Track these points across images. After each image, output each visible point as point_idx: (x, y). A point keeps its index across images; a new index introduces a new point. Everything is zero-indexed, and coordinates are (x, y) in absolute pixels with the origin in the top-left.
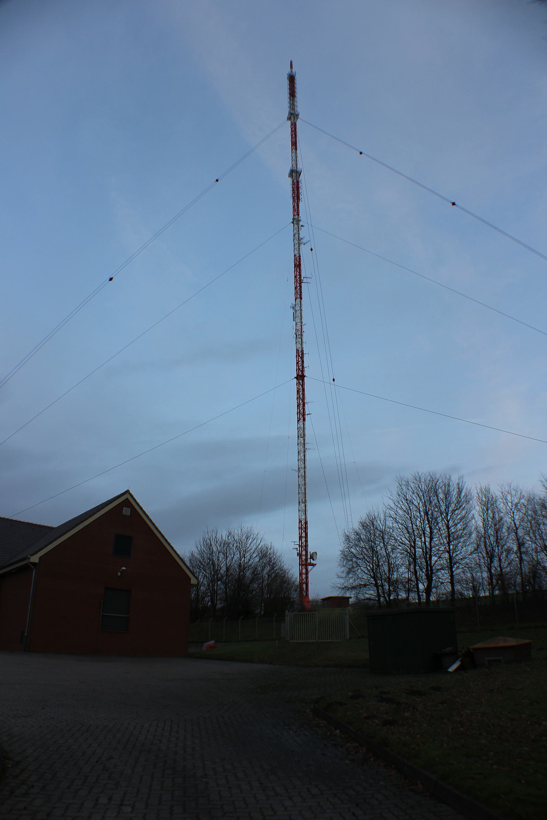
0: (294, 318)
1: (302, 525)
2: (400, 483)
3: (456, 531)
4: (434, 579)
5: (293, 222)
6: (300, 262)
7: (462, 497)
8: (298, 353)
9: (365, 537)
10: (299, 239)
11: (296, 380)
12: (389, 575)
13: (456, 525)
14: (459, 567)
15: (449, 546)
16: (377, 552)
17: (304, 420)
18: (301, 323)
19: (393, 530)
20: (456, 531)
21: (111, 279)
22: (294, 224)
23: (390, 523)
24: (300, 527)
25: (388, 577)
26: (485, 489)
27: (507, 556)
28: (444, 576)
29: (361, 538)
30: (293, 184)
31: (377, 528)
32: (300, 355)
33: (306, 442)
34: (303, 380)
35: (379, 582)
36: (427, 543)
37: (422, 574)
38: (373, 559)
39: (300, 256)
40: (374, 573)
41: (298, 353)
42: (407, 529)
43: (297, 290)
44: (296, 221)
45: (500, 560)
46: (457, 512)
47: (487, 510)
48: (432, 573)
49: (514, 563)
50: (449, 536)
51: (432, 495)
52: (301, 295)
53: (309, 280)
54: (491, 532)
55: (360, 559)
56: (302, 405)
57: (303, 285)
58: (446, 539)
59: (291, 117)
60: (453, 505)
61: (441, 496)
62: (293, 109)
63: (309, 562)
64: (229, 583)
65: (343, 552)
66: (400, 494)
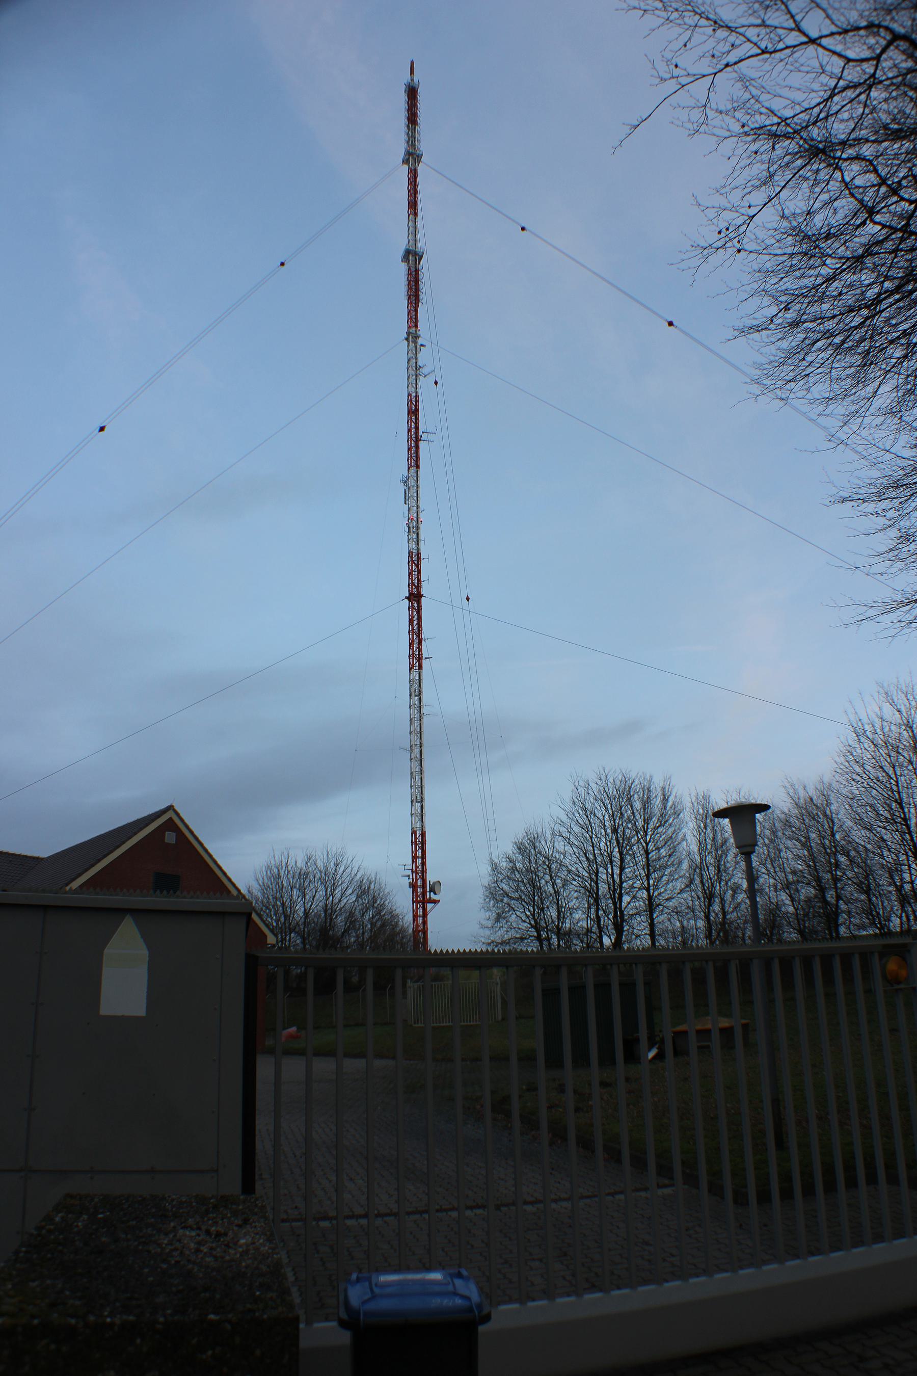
0: (405, 498)
1: (416, 838)
2: (576, 784)
3: (659, 859)
4: (625, 929)
5: (407, 339)
6: (417, 405)
7: (668, 808)
9: (521, 866)
10: (417, 368)
11: (407, 601)
12: (559, 923)
13: (658, 849)
14: (662, 911)
15: (648, 880)
16: (540, 888)
17: (420, 667)
18: (418, 507)
19: (564, 856)
20: (659, 859)
21: (102, 429)
22: (408, 341)
23: (560, 845)
24: (413, 841)
25: (558, 927)
26: (703, 797)
27: (733, 896)
28: (640, 925)
29: (516, 868)
30: (409, 274)
31: (540, 853)
32: (415, 560)
33: (424, 702)
34: (419, 603)
35: (544, 935)
36: (615, 876)
37: (607, 921)
38: (534, 898)
39: (417, 396)
40: (535, 921)
42: (585, 854)
43: (411, 452)
44: (412, 336)
45: (722, 901)
46: (660, 830)
47: (705, 828)
48: (623, 920)
49: (743, 906)
50: (648, 865)
51: (623, 803)
52: (417, 461)
53: (431, 437)
54: (710, 859)
55: (513, 899)
56: (416, 644)
57: (421, 444)
58: (643, 869)
59: (409, 158)
60: (655, 819)
61: (638, 805)
62: (413, 145)
63: (428, 897)
64: (309, 935)
65: (488, 888)
66: (576, 800)
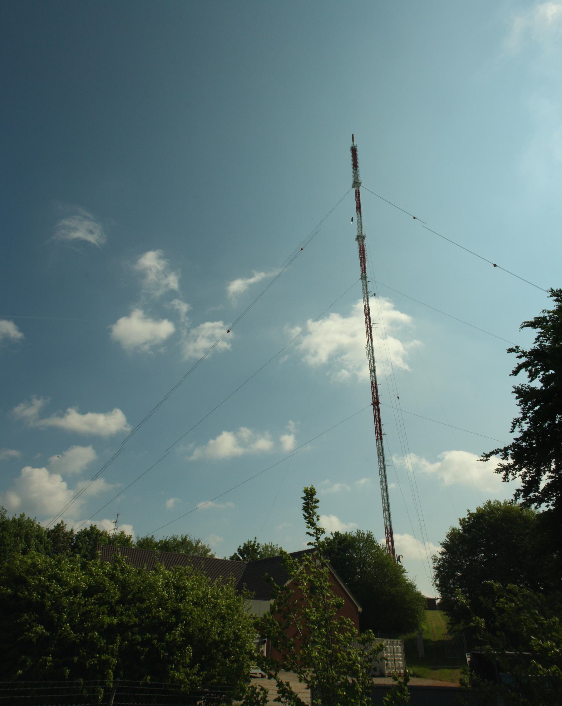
5: (361, 279)
11: (372, 406)
34: (378, 407)
41: (373, 385)
44: (364, 277)
52: (371, 337)
57: (373, 329)
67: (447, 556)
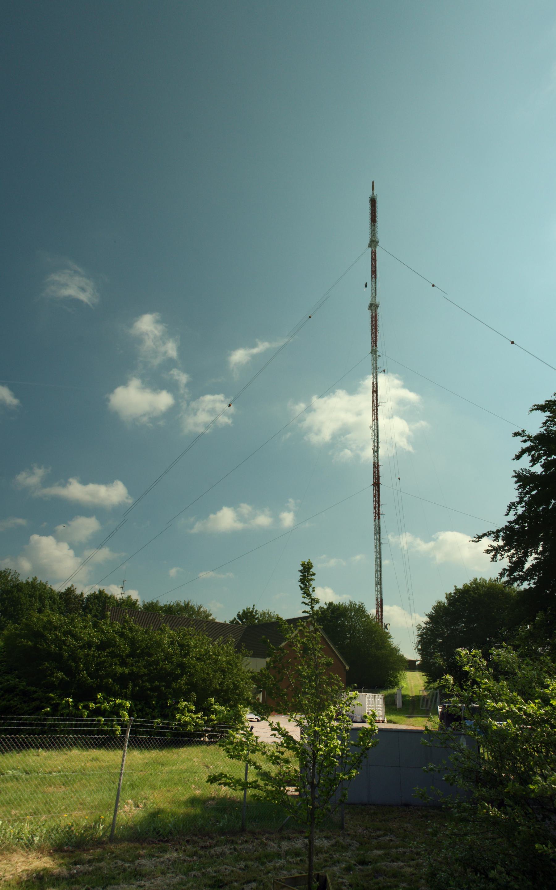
1: (378, 602)
5: (371, 353)
6: (377, 388)
8: (375, 465)
11: (373, 486)
30: (372, 317)
34: (379, 488)
44: (374, 351)
57: (379, 408)
67: (431, 625)
